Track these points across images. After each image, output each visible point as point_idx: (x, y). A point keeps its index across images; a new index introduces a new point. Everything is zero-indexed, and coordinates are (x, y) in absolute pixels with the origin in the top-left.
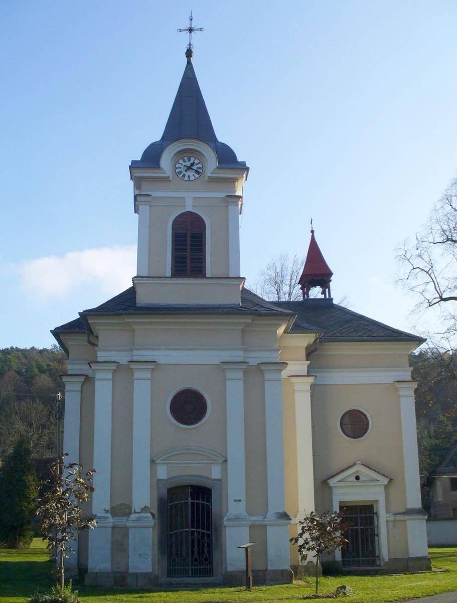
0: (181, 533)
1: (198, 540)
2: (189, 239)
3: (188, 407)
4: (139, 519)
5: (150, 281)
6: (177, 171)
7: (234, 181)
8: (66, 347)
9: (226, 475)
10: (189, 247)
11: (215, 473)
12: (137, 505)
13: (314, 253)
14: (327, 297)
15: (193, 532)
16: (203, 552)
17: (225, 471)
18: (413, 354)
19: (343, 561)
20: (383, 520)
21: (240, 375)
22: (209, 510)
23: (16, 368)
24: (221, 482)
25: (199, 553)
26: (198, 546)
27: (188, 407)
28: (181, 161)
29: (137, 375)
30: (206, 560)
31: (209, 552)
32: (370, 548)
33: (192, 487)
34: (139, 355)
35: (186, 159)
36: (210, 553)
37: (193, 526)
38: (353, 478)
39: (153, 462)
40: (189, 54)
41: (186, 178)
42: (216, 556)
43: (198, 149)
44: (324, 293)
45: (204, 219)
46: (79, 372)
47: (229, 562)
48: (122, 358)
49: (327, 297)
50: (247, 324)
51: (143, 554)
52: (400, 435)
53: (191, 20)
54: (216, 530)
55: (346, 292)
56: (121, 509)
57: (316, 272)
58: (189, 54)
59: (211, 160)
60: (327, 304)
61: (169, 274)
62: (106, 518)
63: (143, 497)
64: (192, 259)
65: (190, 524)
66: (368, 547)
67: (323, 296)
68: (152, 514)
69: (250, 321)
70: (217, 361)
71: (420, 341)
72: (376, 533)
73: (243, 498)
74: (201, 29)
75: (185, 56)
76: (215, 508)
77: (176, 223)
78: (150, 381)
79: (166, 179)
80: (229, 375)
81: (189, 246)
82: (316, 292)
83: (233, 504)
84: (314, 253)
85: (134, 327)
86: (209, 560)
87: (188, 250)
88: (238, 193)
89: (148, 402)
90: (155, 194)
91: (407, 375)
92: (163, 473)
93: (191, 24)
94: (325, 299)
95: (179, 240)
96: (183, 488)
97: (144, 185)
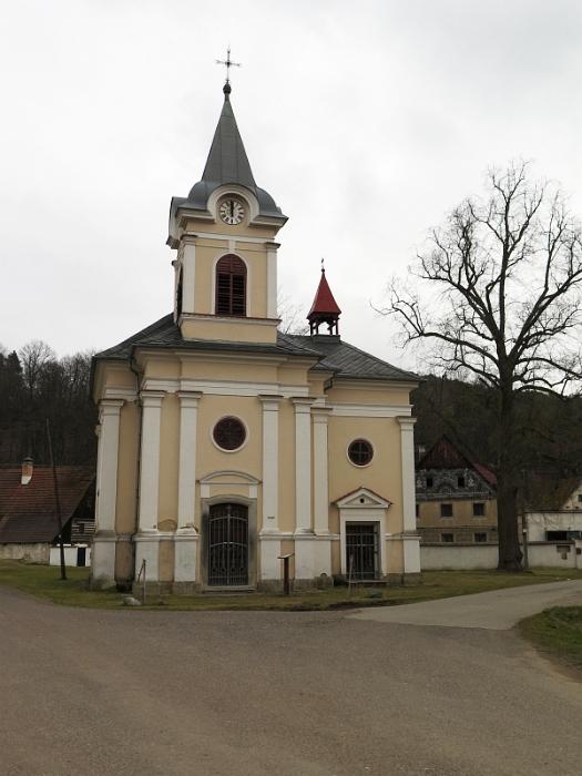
2: (231, 280)
3: (229, 433)
5: (196, 317)
7: (276, 229)
10: (231, 288)
11: (252, 493)
12: (182, 523)
13: (324, 291)
14: (334, 333)
15: (231, 545)
17: (261, 492)
18: (522, 549)
20: (384, 534)
21: (308, 409)
22: (245, 524)
24: (259, 500)
27: (229, 433)
29: (184, 403)
34: (186, 386)
36: (246, 563)
38: (358, 501)
39: (198, 482)
40: (227, 90)
41: (229, 222)
44: (330, 329)
45: (243, 258)
46: (118, 397)
47: (263, 572)
48: (171, 388)
49: (334, 333)
50: (283, 363)
51: (188, 567)
52: (398, 452)
54: (252, 543)
55: (351, 331)
56: (170, 524)
57: (325, 309)
58: (227, 90)
59: (254, 210)
60: (335, 340)
61: (213, 312)
62: (154, 532)
63: (189, 515)
67: (328, 333)
68: (197, 530)
69: (285, 359)
70: (394, 415)
76: (251, 525)
78: (195, 410)
80: (266, 407)
81: (232, 288)
82: (324, 329)
83: (267, 523)
84: (324, 291)
85: (182, 359)
88: (277, 240)
89: (194, 426)
90: (200, 235)
91: (408, 412)
92: (206, 492)
94: (331, 336)
95: (222, 280)
97: (189, 226)
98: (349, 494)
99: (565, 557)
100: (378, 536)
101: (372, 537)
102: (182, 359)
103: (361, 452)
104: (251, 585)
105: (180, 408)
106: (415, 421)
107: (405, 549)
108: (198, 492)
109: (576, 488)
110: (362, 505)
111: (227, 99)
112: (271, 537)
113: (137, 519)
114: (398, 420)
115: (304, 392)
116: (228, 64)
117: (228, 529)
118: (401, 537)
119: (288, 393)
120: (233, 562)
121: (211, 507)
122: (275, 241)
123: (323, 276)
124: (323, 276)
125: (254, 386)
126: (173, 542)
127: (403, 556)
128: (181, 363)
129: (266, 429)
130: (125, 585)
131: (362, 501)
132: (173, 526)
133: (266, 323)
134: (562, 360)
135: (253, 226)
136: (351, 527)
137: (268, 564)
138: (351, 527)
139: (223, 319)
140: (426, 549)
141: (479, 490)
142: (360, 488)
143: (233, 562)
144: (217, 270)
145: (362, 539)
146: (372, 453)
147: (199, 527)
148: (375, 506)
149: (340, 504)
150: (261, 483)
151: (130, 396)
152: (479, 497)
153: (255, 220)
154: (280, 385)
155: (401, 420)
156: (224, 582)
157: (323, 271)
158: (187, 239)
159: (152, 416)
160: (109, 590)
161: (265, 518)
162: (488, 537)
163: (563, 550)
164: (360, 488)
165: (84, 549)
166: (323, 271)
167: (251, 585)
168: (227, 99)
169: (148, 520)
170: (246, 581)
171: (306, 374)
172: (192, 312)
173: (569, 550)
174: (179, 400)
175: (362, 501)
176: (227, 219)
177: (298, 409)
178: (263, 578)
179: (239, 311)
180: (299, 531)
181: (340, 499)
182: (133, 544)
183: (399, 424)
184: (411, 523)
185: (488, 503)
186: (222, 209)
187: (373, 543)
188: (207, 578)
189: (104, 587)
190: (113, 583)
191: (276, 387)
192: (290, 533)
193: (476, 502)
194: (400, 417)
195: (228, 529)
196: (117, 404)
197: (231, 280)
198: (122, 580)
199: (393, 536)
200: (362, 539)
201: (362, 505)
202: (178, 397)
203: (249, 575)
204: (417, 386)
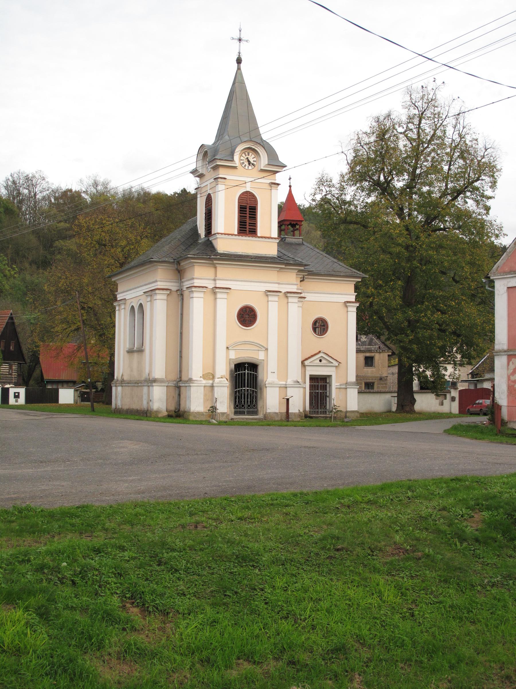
0: (242, 390)
1: (251, 394)
2: (248, 210)
3: (247, 316)
4: (220, 381)
5: (226, 236)
6: (241, 162)
8: (443, 418)
9: (267, 358)
10: (248, 215)
12: (218, 374)
15: (248, 390)
16: (241, 402)
19: (310, 411)
20: (335, 384)
23: (57, 243)
25: (250, 402)
26: (250, 399)
27: (247, 316)
28: (244, 155)
29: (219, 296)
30: (254, 406)
31: (256, 401)
32: (325, 404)
33: (248, 363)
34: (219, 284)
35: (247, 153)
37: (248, 387)
39: (227, 348)
40: (239, 61)
42: (260, 404)
43: (256, 149)
51: (224, 405)
53: (240, 31)
54: (261, 389)
58: (239, 61)
59: (264, 161)
61: (236, 233)
62: (201, 381)
63: (223, 370)
64: (249, 223)
65: (246, 385)
66: (323, 403)
69: (284, 266)
71: (447, 432)
72: (328, 394)
73: (276, 371)
74: (247, 41)
75: (236, 62)
76: (260, 377)
77: (241, 198)
79: (235, 167)
80: (270, 298)
83: (270, 377)
85: (217, 265)
86: (255, 406)
87: (248, 217)
89: (226, 311)
91: (353, 298)
93: (240, 34)
95: (242, 209)
96: (244, 364)
98: (312, 356)
99: (442, 404)
100: (330, 386)
101: (326, 385)
102: (217, 265)
103: (320, 326)
104: (260, 416)
105: (216, 299)
106: (358, 305)
107: (165, 404)
108: (227, 355)
109: (510, 413)
110: (320, 364)
111: (239, 69)
112: (273, 385)
113: (181, 371)
114: (346, 303)
115: (294, 288)
116: (240, 40)
117: (246, 378)
118: (347, 385)
119: (284, 289)
120: (249, 400)
121: (235, 365)
122: (277, 182)
123: (290, 192)
124: (290, 192)
125: (262, 284)
126: (212, 387)
127: (347, 399)
128: (216, 268)
129: (269, 313)
130: (178, 414)
131: (320, 361)
132: (211, 377)
133: (270, 240)
134: (415, 109)
135: (262, 171)
136: (313, 378)
137: (271, 402)
138: (313, 378)
139: (244, 238)
140: (360, 394)
141: (370, 344)
142: (320, 352)
143: (249, 400)
144: (239, 203)
145: (319, 386)
146: (327, 328)
147: (228, 378)
148: (329, 365)
149: (307, 363)
150: (267, 349)
151: (173, 286)
152: (370, 351)
153: (264, 167)
154: (279, 283)
155: (348, 304)
156: (243, 413)
157: (290, 186)
158: (219, 180)
159: (197, 304)
160: (164, 417)
161: (269, 372)
162: (375, 386)
163: (441, 398)
164: (320, 352)
165: (8, 389)
166: (290, 186)
167: (260, 416)
168: (239, 69)
169: (196, 370)
170: (256, 413)
171: (295, 274)
172: (223, 232)
173: (446, 399)
174: (215, 293)
175: (320, 361)
176: (243, 163)
177: (290, 300)
178: (268, 411)
179: (253, 232)
180: (290, 381)
181: (306, 359)
182: (179, 388)
183: (347, 307)
184: (352, 378)
185: (377, 356)
186: (242, 158)
187: (326, 390)
188: (233, 410)
189: (160, 415)
190: (166, 414)
191: (277, 285)
192: (284, 383)
193: (368, 355)
194: (348, 302)
195: (246, 378)
196: (165, 292)
197: (248, 210)
198: (170, 412)
199: (341, 385)
200: (319, 386)
201: (320, 364)
202: (215, 290)
203: (259, 409)
204: (360, 280)
